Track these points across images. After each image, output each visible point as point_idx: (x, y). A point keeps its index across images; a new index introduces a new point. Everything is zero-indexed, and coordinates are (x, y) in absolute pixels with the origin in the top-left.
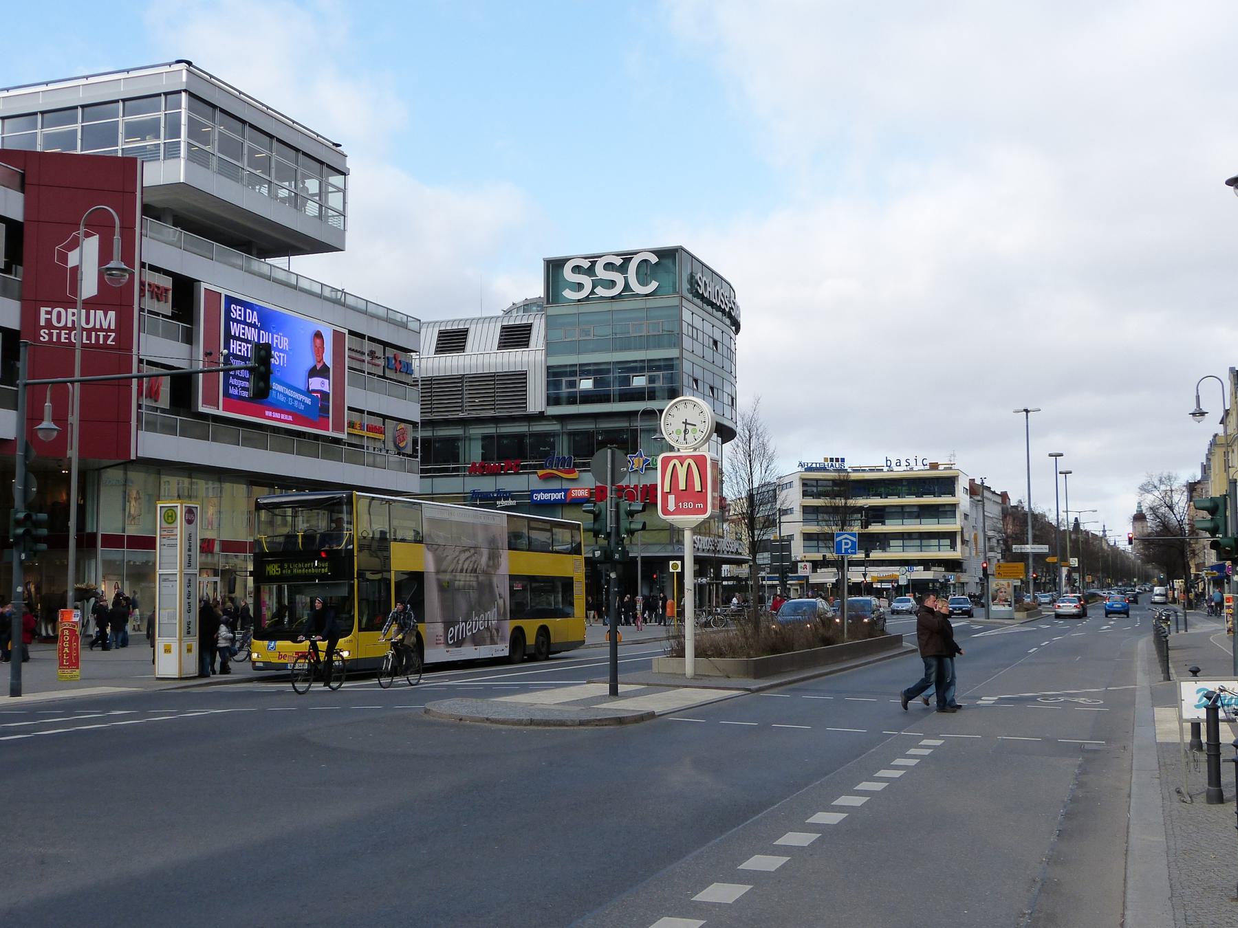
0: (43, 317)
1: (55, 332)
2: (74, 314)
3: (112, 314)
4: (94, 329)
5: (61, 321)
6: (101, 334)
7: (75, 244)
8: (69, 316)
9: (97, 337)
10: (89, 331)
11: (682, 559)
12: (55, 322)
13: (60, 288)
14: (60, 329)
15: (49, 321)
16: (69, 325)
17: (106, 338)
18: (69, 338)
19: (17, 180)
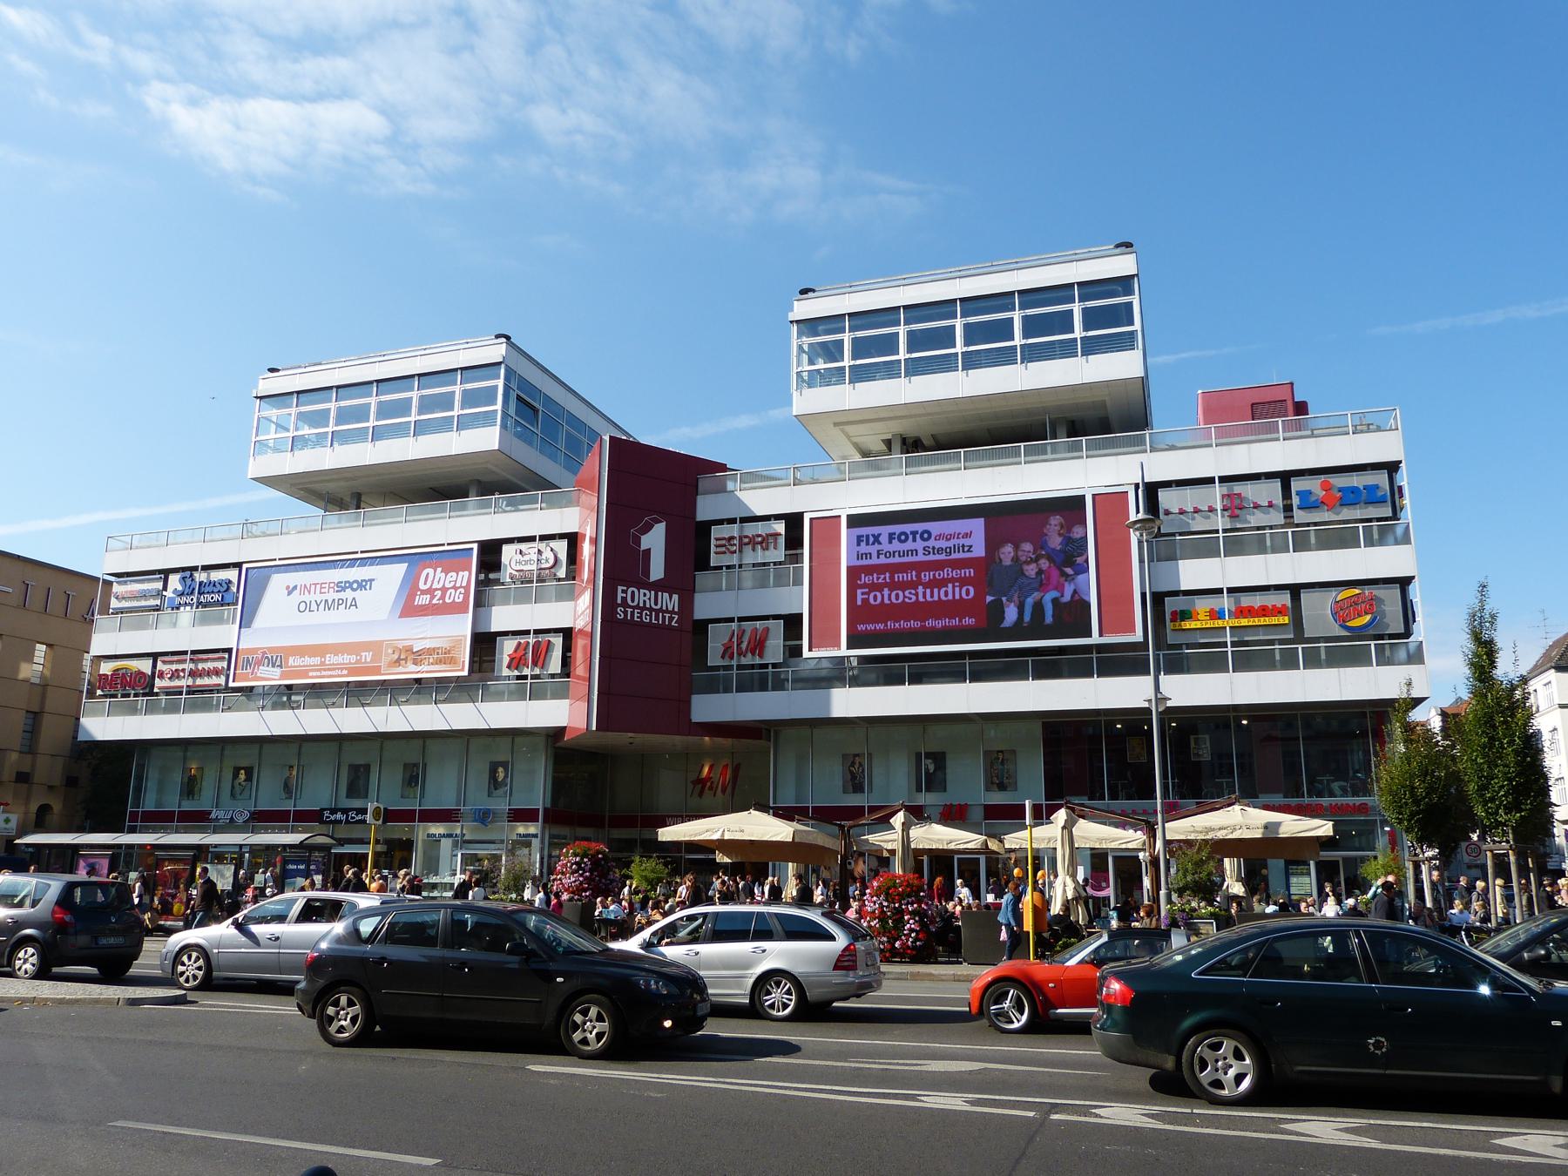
0: (620, 595)
3: (675, 597)
7: (647, 528)
8: (643, 597)
10: (658, 612)
15: (624, 599)
17: (671, 619)
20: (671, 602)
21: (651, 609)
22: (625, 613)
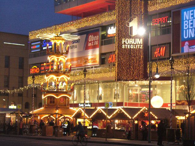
0: (123, 41)
4: (136, 44)
6: (139, 45)
12: (126, 43)
15: (125, 43)
17: (140, 46)
21: (133, 44)
22: (125, 46)
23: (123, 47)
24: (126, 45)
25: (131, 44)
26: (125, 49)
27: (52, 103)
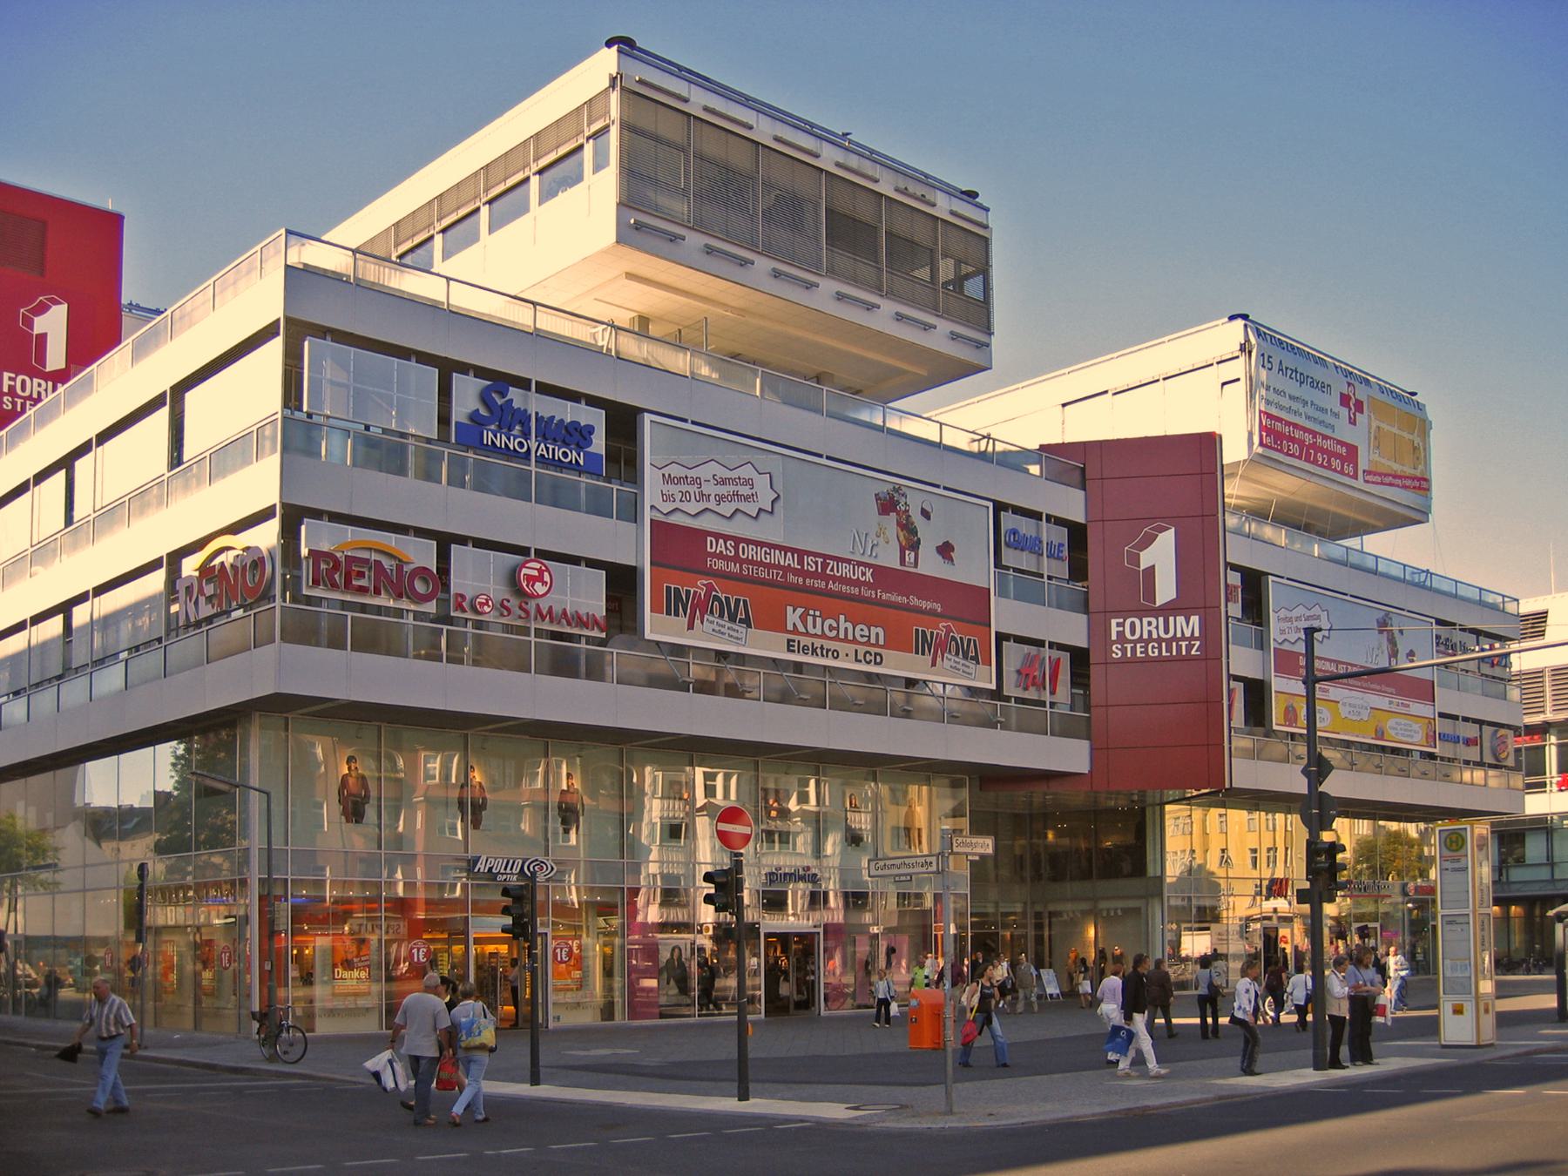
0: (1114, 629)
1: (1129, 646)
2: (1150, 624)
3: (1195, 619)
4: (1174, 638)
5: (1135, 634)
6: (1184, 644)
7: (1149, 541)
8: (1149, 626)
9: (1179, 648)
10: (1169, 642)
11: (1300, 458)
12: (1128, 636)
13: (1136, 594)
14: (25, 398)
15: (1121, 634)
16: (1145, 636)
17: (1189, 648)
18: (1146, 652)
19: (1077, 476)
20: (1190, 626)
21: (1159, 640)
22: (1124, 650)
23: (1117, 653)
24: (19, 401)
25: (1150, 639)
26: (1124, 661)
27: (1436, 1019)
